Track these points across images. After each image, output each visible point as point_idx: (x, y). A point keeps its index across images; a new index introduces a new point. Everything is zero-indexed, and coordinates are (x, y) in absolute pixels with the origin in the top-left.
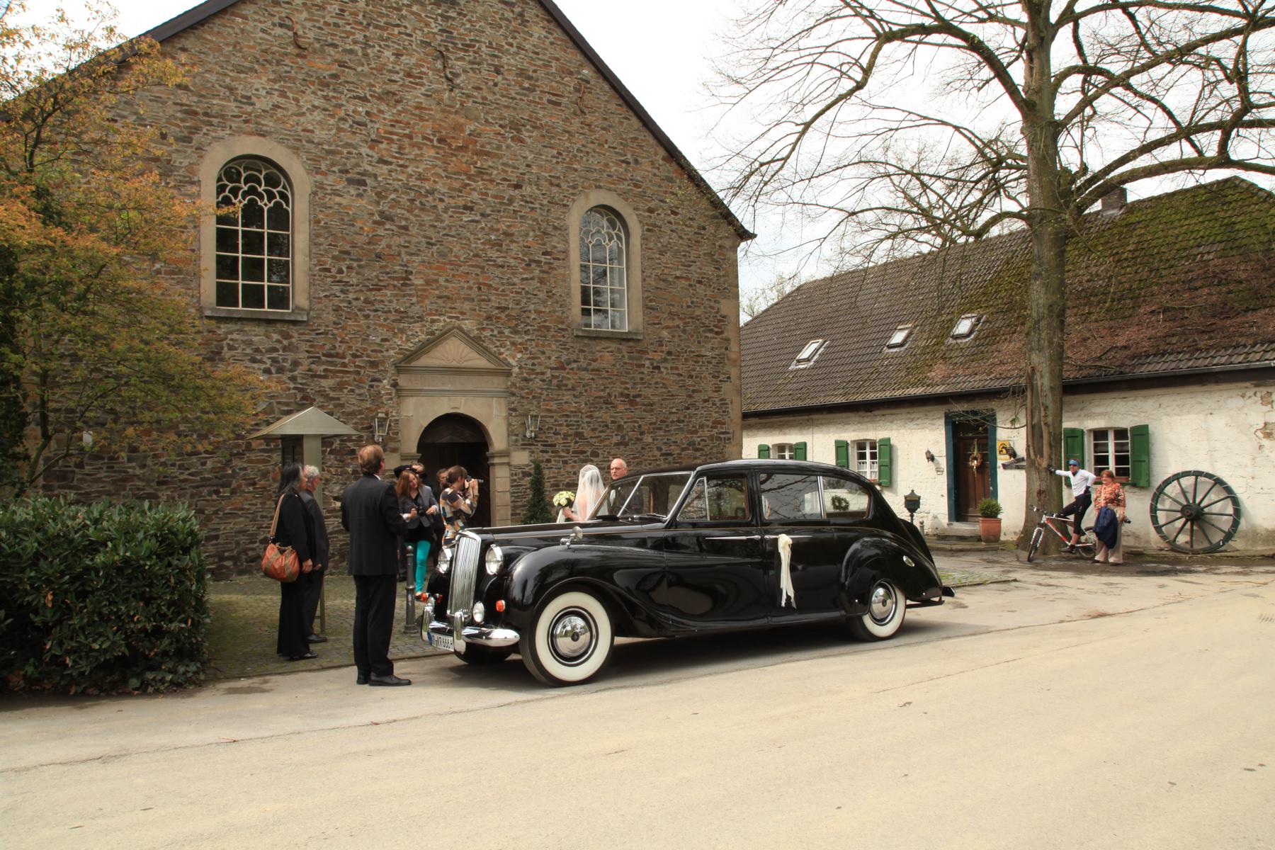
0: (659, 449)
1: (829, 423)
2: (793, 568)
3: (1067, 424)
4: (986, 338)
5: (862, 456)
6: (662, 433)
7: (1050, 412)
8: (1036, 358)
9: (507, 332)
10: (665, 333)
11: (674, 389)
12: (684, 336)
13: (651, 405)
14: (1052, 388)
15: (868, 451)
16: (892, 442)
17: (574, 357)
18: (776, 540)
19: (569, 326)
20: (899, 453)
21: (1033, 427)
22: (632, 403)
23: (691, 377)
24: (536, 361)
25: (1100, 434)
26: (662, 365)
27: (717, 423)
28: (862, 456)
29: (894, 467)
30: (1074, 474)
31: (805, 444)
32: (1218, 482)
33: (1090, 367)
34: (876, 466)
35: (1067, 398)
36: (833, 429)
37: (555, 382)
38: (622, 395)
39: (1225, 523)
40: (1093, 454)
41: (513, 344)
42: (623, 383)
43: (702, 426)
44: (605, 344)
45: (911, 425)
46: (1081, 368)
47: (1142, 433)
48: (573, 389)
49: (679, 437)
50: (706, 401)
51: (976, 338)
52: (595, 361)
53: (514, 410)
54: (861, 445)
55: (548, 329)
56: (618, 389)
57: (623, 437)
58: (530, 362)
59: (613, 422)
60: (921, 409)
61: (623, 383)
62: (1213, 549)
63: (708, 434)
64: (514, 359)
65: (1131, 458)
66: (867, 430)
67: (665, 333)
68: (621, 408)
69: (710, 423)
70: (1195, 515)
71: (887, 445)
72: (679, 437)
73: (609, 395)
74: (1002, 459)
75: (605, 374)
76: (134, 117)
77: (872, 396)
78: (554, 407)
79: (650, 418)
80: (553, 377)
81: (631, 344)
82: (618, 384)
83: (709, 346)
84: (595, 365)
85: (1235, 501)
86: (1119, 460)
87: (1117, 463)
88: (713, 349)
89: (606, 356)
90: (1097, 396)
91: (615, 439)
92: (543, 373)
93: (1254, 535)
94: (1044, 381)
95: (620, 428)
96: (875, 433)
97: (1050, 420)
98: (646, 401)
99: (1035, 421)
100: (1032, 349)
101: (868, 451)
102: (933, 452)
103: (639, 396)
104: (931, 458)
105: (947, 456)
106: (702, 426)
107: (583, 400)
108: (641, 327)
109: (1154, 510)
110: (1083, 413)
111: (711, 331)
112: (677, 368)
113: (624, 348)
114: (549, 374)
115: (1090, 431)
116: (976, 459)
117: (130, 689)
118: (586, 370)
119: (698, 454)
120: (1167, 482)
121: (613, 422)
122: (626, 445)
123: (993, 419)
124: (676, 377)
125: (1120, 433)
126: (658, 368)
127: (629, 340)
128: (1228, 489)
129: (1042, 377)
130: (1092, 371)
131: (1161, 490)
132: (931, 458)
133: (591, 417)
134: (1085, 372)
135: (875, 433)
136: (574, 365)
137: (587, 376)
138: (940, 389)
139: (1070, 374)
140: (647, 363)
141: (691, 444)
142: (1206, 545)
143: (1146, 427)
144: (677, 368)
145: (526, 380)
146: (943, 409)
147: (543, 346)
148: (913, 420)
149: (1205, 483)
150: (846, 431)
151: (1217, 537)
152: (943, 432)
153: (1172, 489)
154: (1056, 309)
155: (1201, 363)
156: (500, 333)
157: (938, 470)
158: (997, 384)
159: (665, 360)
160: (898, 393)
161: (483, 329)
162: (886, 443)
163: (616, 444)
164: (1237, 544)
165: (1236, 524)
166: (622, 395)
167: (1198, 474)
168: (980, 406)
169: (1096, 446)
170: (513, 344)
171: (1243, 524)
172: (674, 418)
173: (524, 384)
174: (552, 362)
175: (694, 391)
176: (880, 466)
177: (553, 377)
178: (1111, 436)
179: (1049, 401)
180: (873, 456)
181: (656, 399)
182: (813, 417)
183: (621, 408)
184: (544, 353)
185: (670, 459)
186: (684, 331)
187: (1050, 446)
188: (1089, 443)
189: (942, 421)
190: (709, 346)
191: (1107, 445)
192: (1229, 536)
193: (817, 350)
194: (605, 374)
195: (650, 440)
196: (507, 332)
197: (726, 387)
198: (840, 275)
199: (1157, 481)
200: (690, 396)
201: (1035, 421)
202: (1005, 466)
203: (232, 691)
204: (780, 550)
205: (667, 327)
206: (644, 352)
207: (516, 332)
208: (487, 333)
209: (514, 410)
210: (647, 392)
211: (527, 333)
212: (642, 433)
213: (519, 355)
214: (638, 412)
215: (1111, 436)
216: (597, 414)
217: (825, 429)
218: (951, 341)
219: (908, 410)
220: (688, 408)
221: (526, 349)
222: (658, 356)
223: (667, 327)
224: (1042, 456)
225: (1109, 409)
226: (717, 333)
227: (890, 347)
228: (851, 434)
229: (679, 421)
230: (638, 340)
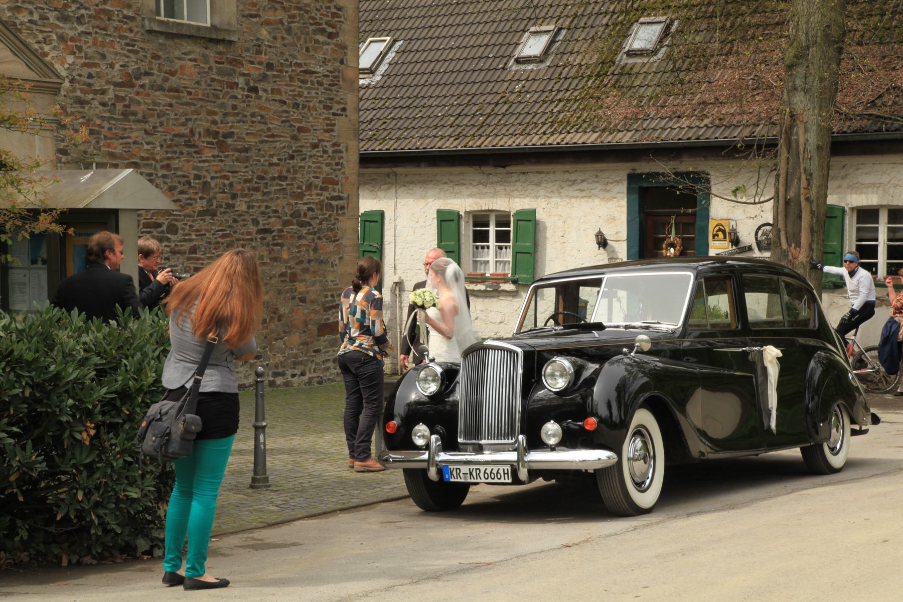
0: (255, 222)
1: (425, 182)
2: (778, 389)
3: (832, 200)
4: (683, 63)
5: (481, 237)
6: (258, 196)
7: (815, 183)
8: (800, 101)
9: (52, 16)
10: (264, 33)
11: (275, 125)
12: (289, 39)
13: (246, 150)
14: (819, 148)
15: (492, 230)
16: (539, 216)
17: (144, 66)
18: (761, 353)
19: (137, 12)
20: (549, 234)
21: (787, 203)
22: (222, 146)
23: (296, 106)
24: (93, 71)
25: (867, 215)
26: (260, 86)
27: (330, 182)
28: (481, 237)
29: (539, 255)
30: (852, 274)
31: (382, 214)
33: (861, 116)
34: (508, 256)
35: (838, 161)
36: (433, 191)
37: (120, 106)
38: (208, 132)
40: (471, 228)
41: (61, 38)
42: (210, 113)
43: (309, 187)
44: (187, 46)
45: (571, 191)
46: (847, 118)
48: (144, 120)
49: (280, 204)
50: (315, 146)
51: (669, 57)
52: (173, 74)
53: (64, 152)
54: (480, 220)
55: (109, 14)
56: (202, 124)
57: (210, 201)
58: (86, 71)
59: (197, 177)
60: (589, 166)
61: (210, 113)
63: (316, 199)
64: (63, 64)
66: (495, 195)
67: (264, 33)
68: (208, 154)
69: (318, 182)
71: (529, 221)
72: (280, 204)
73: (192, 132)
75: (186, 98)
77: (508, 143)
78: (118, 151)
79: (245, 172)
80: (118, 98)
81: (221, 48)
82: (203, 115)
83: (320, 56)
84: (174, 81)
87: (889, 257)
88: (325, 61)
89: (189, 64)
90: (869, 160)
91: (200, 205)
92: (104, 92)
94: (809, 137)
95: (206, 186)
96: (509, 201)
97: (813, 193)
98: (240, 145)
99: (791, 194)
100: (795, 88)
101: (492, 230)
102: (608, 234)
103: (231, 135)
105: (628, 240)
106: (309, 187)
107: (157, 139)
108: (234, 21)
110: (845, 183)
111: (322, 31)
112: (279, 92)
113: (211, 54)
114: (111, 95)
115: (852, 209)
116: (672, 245)
117: (139, 554)
118: (161, 88)
119: (304, 231)
121: (197, 177)
122: (213, 214)
123: (701, 179)
124: (277, 107)
126: (254, 90)
127: (217, 41)
129: (806, 130)
130: (865, 122)
133: (168, 167)
134: (856, 124)
135: (509, 201)
136: (146, 80)
137: (163, 98)
138: (625, 138)
140: (241, 81)
141: (296, 214)
144: (279, 92)
145: (81, 102)
146: (622, 171)
147: (103, 44)
148: (574, 182)
150: (456, 195)
152: (624, 203)
154: (835, 32)
156: (43, 18)
158: (719, 135)
159: (264, 78)
160: (554, 140)
161: (18, 9)
162: (528, 218)
163: (202, 213)
166: (208, 132)
168: (688, 165)
169: (858, 229)
170: (61, 38)
172: (274, 172)
173: (77, 108)
174: (116, 74)
175: (300, 130)
176: (516, 254)
177: (118, 98)
178: (883, 217)
179: (814, 166)
180: (502, 237)
181: (253, 140)
182: (399, 170)
183: (208, 154)
184: (103, 57)
185: (269, 237)
186: (289, 30)
187: (812, 231)
188: (851, 225)
189: (623, 187)
190: (320, 56)
191: (876, 230)
193: (383, 55)
194: (186, 98)
195: (244, 207)
196: (52, 16)
197: (341, 123)
200: (295, 138)
201: (791, 194)
203: (142, 570)
204: (767, 364)
205: (268, 23)
206: (236, 62)
207: (65, 19)
208: (24, 17)
209: (64, 152)
210: (241, 129)
211: (80, 20)
212: (234, 196)
213: (70, 59)
214: (228, 162)
215: (883, 217)
216: (175, 163)
217: (418, 190)
218: (626, 60)
219: (568, 167)
220: (292, 157)
221: (80, 48)
222: (255, 71)
223: (268, 23)
224: (798, 245)
225: (885, 179)
226: (331, 36)
227: (631, 54)
229: (282, 178)
230: (230, 42)
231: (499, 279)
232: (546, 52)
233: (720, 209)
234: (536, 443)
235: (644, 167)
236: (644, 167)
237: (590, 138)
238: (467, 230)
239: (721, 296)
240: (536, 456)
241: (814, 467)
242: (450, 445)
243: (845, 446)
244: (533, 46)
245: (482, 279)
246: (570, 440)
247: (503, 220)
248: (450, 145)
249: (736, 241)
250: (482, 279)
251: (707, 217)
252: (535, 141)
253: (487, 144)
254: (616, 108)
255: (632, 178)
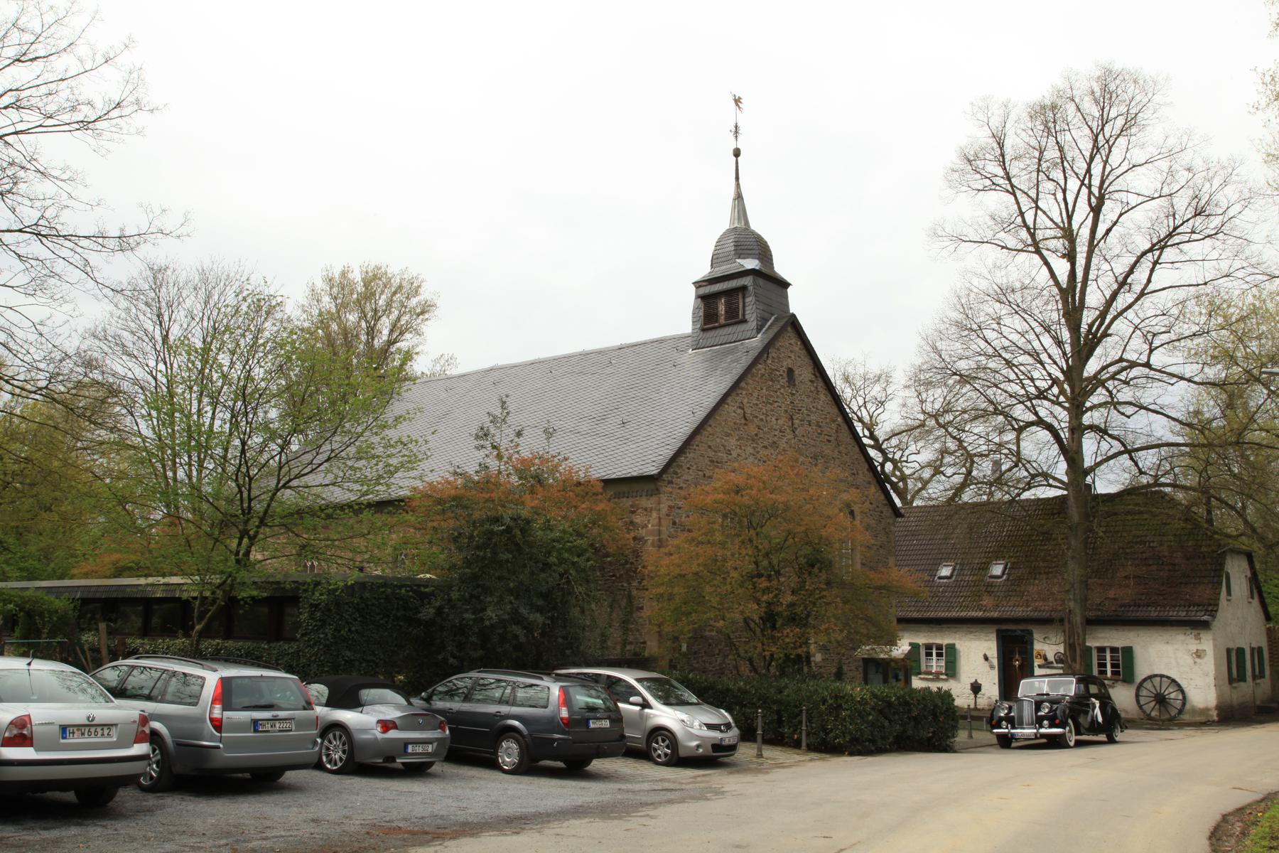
4: (1014, 583)
25: (1101, 650)
28: (929, 655)
32: (1174, 681)
34: (943, 663)
35: (1088, 627)
39: (1178, 704)
45: (971, 636)
47: (1128, 652)
51: (1008, 580)
54: (929, 647)
62: (1172, 719)
65: (1124, 664)
70: (1161, 700)
71: (951, 648)
74: (1037, 662)
76: (1069, 687)
85: (1183, 692)
86: (1113, 666)
93: (1195, 711)
94: (1078, 619)
96: (944, 640)
102: (989, 655)
104: (986, 658)
109: (1137, 696)
120: (1145, 680)
123: (1031, 634)
125: (1114, 650)
128: (1179, 685)
131: (1141, 684)
132: (986, 658)
135: (944, 640)
138: (996, 615)
139: (1091, 614)
142: (1167, 716)
143: (1131, 648)
146: (994, 628)
149: (1166, 682)
151: (1174, 712)
153: (1148, 685)
155: (1164, 615)
157: (992, 667)
160: (963, 614)
164: (1186, 717)
165: (1184, 704)
167: (1162, 676)
171: (1188, 707)
178: (1108, 651)
179: (1080, 630)
180: (939, 655)
188: (1095, 654)
189: (994, 635)
192: (1181, 712)
198: (1138, 488)
199: (1138, 679)
202: (1040, 666)
215: (1108, 651)
227: (940, 578)
228: (921, 640)
231: (938, 674)
232: (1003, 573)
233: (1038, 646)
234: (1041, 727)
235: (1004, 627)
236: (1004, 627)
237: (980, 614)
238: (923, 652)
239: (996, 687)
240: (1042, 730)
241: (1111, 741)
242: (1013, 727)
243: (1119, 736)
244: (945, 572)
245: (931, 673)
246: (1050, 727)
247: (939, 647)
248: (915, 615)
249: (1046, 659)
250: (931, 673)
251: (1032, 649)
252: (954, 614)
253: (932, 615)
254: (987, 601)
255: (998, 632)
